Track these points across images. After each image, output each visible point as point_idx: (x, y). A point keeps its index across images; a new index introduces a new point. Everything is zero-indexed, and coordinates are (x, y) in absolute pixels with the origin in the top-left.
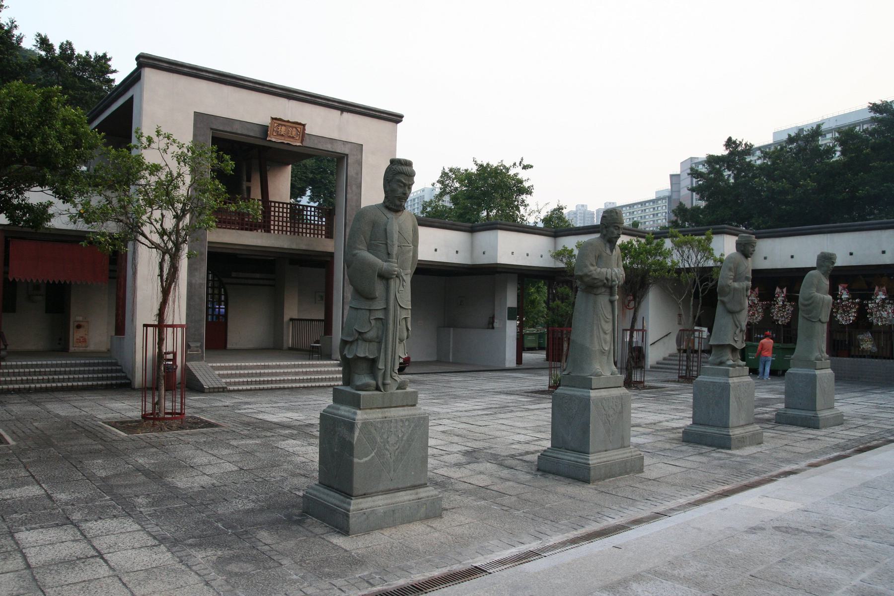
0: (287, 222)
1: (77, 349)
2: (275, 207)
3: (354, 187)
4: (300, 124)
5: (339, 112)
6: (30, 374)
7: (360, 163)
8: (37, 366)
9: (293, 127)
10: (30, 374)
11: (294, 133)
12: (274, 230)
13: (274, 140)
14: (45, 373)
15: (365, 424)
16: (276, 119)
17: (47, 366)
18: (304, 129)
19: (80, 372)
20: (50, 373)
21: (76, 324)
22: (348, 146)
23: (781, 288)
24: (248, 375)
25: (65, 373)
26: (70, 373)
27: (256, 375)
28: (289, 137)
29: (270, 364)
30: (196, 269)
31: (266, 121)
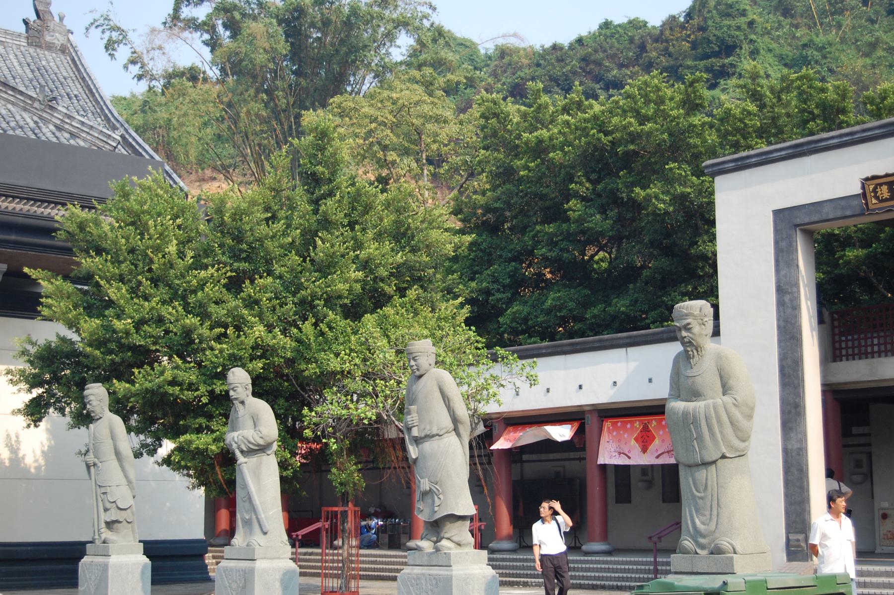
16: (867, 179)
21: (881, 512)
30: (791, 429)
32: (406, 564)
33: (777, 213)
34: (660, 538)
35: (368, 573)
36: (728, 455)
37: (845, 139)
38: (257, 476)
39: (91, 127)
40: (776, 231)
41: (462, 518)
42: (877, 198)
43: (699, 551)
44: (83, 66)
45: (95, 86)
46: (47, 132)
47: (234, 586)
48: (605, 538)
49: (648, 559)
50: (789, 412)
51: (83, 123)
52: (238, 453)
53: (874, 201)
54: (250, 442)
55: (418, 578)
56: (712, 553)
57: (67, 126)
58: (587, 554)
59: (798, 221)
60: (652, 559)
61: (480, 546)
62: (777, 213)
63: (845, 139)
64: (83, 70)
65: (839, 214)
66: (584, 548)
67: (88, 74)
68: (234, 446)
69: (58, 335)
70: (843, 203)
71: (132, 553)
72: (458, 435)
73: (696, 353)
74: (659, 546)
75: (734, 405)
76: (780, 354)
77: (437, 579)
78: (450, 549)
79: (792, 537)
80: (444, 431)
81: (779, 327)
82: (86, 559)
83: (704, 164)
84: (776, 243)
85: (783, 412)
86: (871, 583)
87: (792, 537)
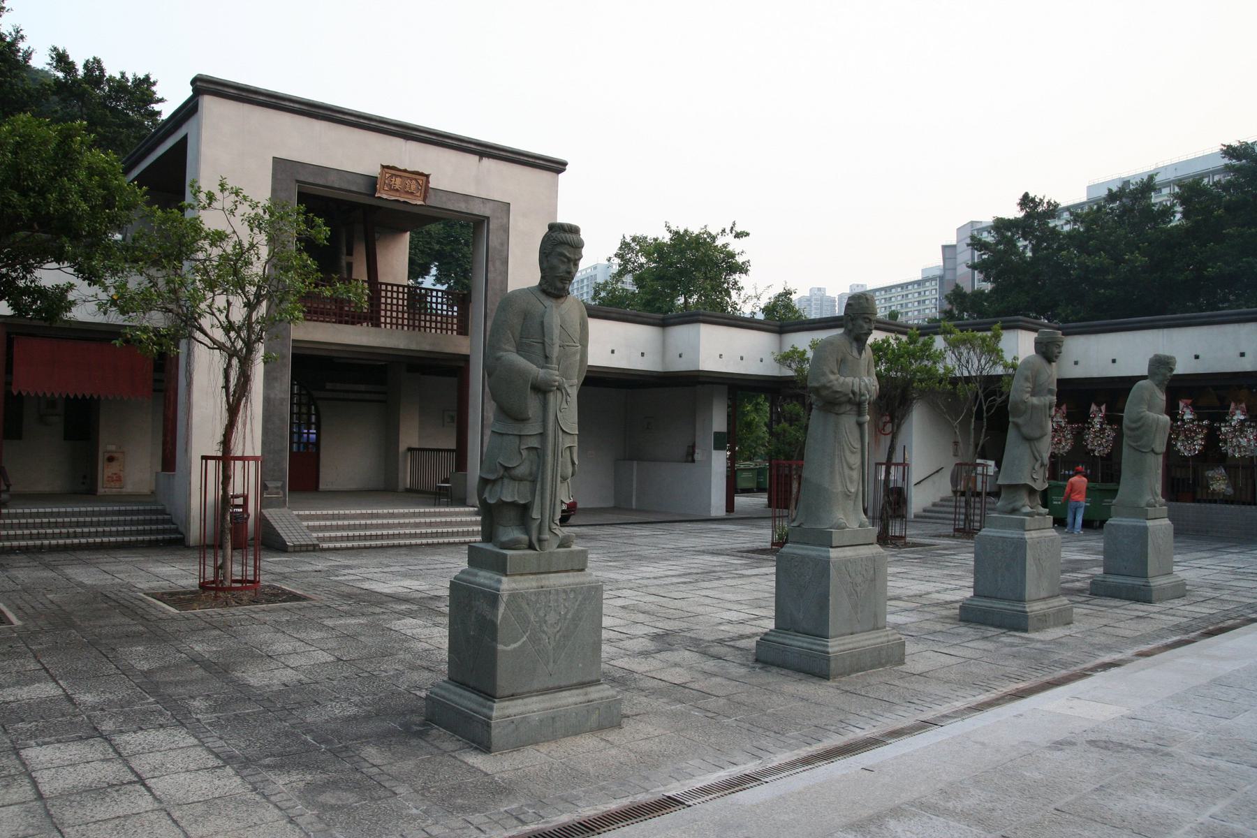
0: (403, 312)
1: (108, 491)
2: (386, 291)
3: (498, 264)
4: (422, 174)
5: (477, 158)
6: (42, 525)
7: (506, 230)
8: (52, 514)
9: (411, 179)
10: (42, 525)
11: (413, 187)
12: (385, 323)
13: (385, 196)
14: (64, 525)
15: (514, 596)
16: (388, 167)
17: (66, 514)
18: (428, 182)
19: (112, 523)
20: (71, 525)
21: (107, 455)
22: (490, 205)
23: (1099, 405)
24: (349, 527)
25: (91, 524)
26: (99, 524)
27: (361, 527)
28: (407, 192)
29: (380, 511)
30: (275, 379)
31: (375, 170)
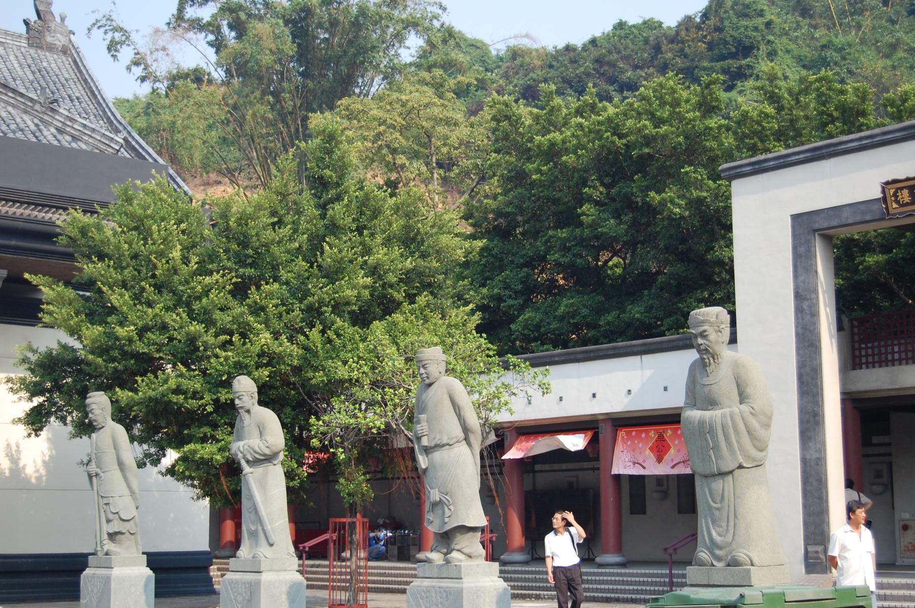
16: (887, 183)
21: (902, 523)
30: (810, 438)
32: (415, 576)
33: (796, 218)
34: (675, 550)
35: (376, 586)
36: (745, 465)
37: (865, 142)
38: (263, 486)
39: (93, 130)
40: (794, 236)
41: (473, 529)
42: (897, 202)
43: (715, 563)
44: (85, 67)
45: (97, 87)
46: (48, 135)
47: (240, 598)
48: (619, 550)
49: (664, 572)
50: (808, 421)
51: (85, 126)
52: (243, 463)
53: (895, 205)
54: (256, 452)
55: (428, 590)
56: (729, 565)
57: (68, 129)
58: (600, 566)
59: (817, 226)
60: (668, 572)
61: (491, 557)
62: (796, 218)
63: (865, 142)
64: (84, 72)
65: (859, 218)
66: (598, 560)
67: (90, 76)
68: (240, 456)
69: (59, 343)
70: (863, 207)
71: (135, 565)
72: (469, 444)
73: (712, 361)
74: (675, 558)
75: (752, 413)
76: (798, 362)
77: (447, 592)
78: (461, 561)
79: (810, 549)
80: (455, 440)
81: (797, 334)
82: (88, 571)
83: (720, 168)
84: (795, 248)
85: (802, 421)
86: (892, 596)
87: (810, 549)
